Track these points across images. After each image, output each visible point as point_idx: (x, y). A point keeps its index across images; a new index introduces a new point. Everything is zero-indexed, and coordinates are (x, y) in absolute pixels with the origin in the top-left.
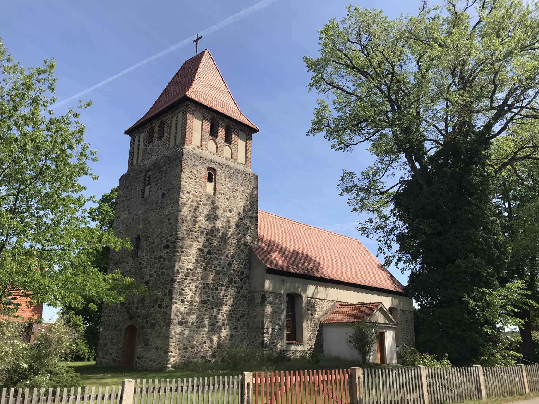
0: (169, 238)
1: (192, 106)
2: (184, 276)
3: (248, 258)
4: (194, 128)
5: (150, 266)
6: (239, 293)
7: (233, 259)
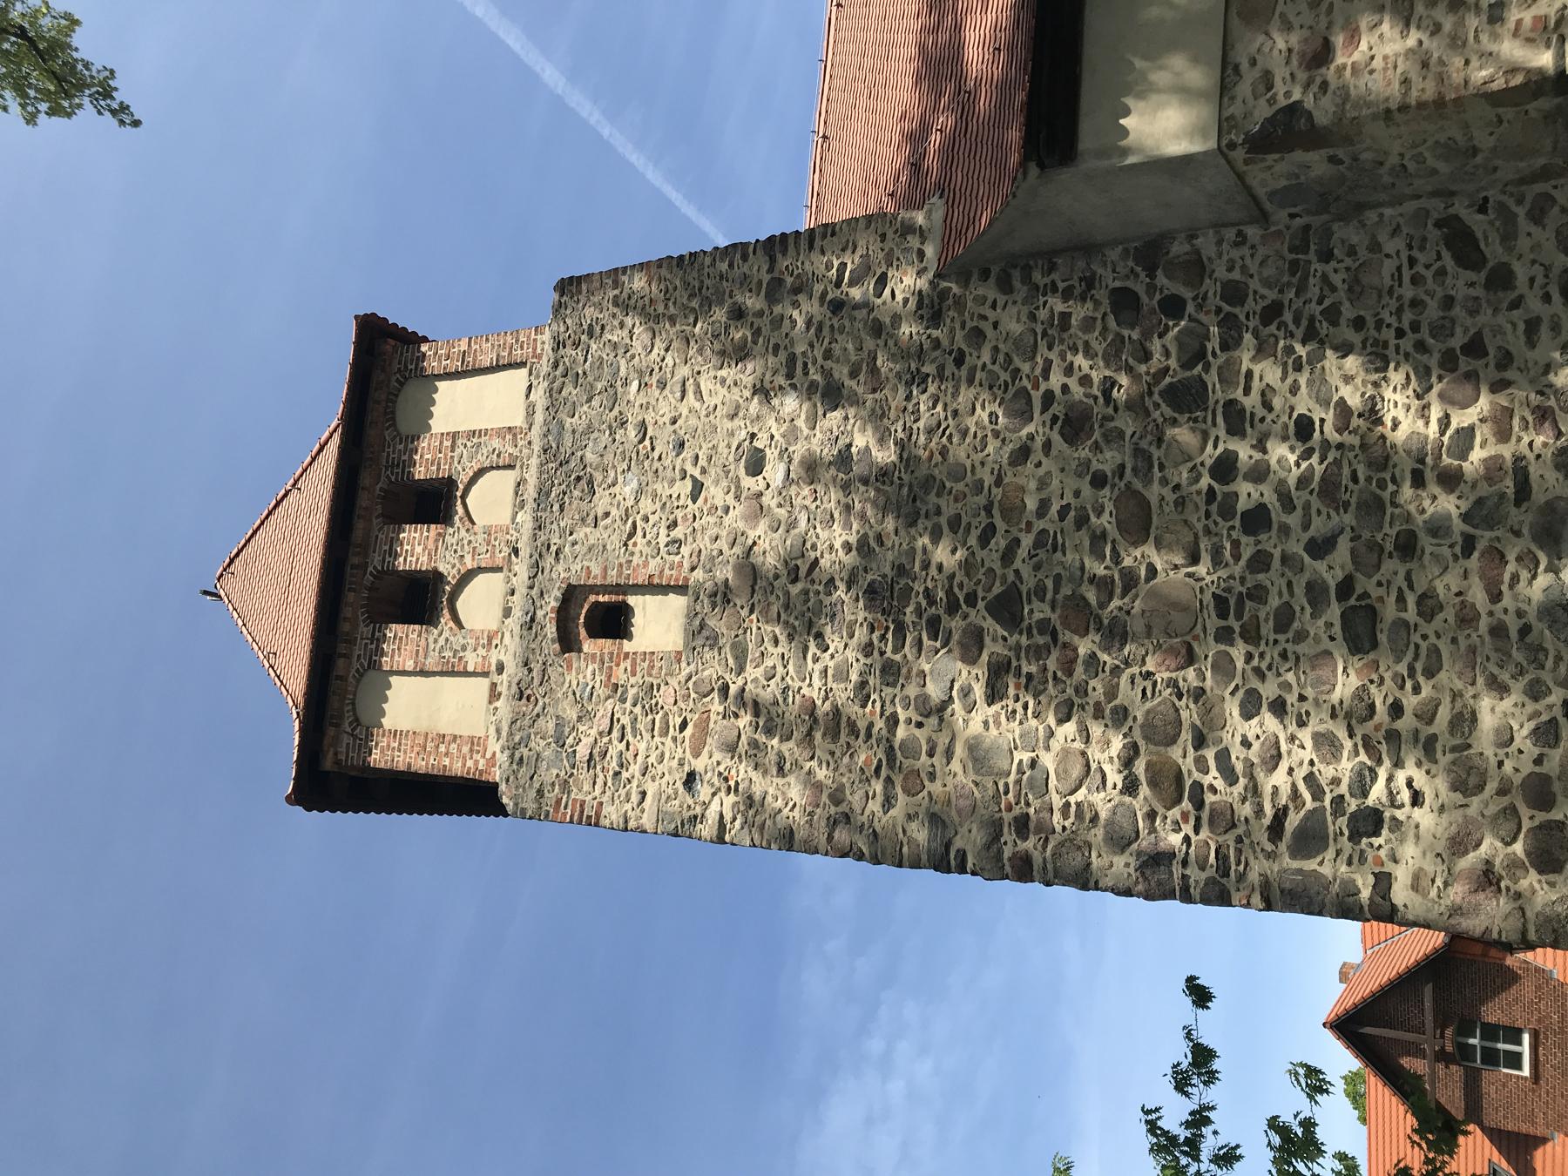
1: (336, 740)
2: (1175, 813)
3: (1016, 275)
4: (422, 727)
6: (1272, 313)
7: (1036, 397)
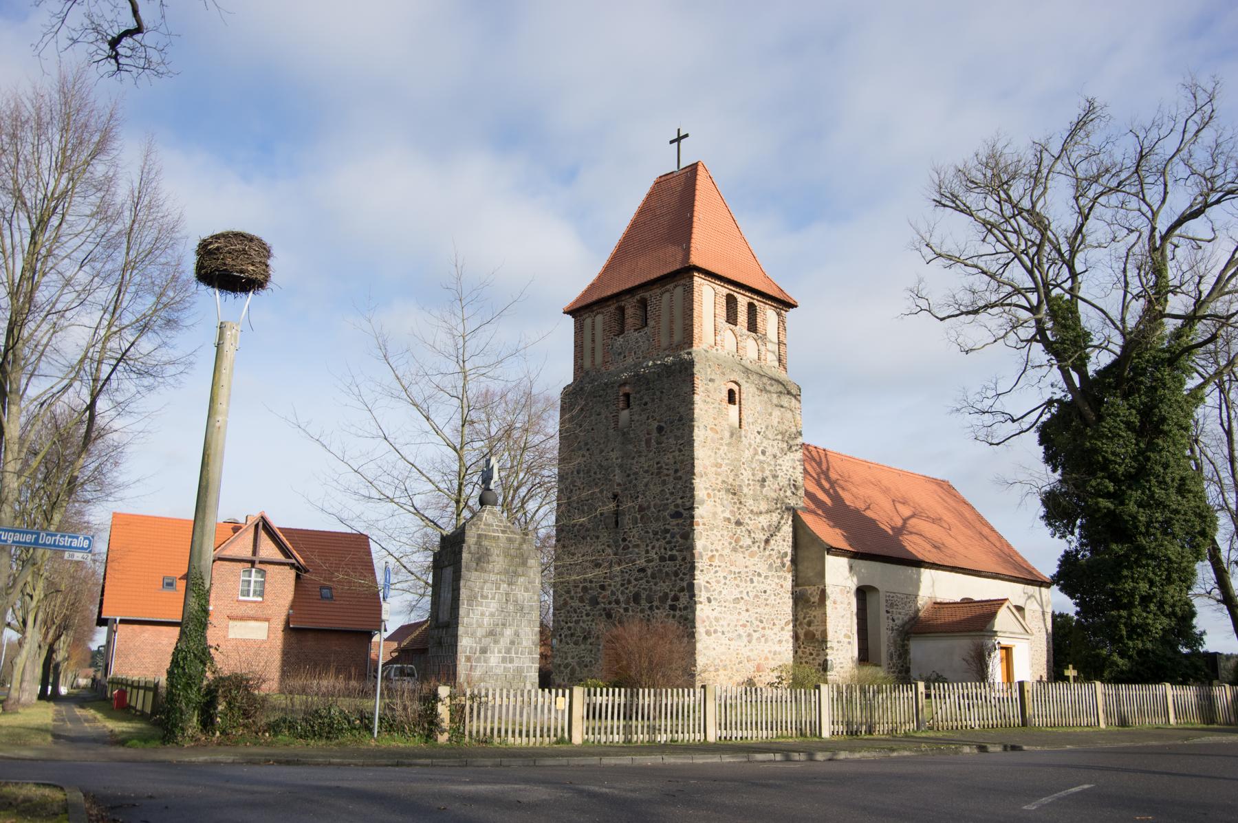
0: (679, 501)
5: (645, 544)
